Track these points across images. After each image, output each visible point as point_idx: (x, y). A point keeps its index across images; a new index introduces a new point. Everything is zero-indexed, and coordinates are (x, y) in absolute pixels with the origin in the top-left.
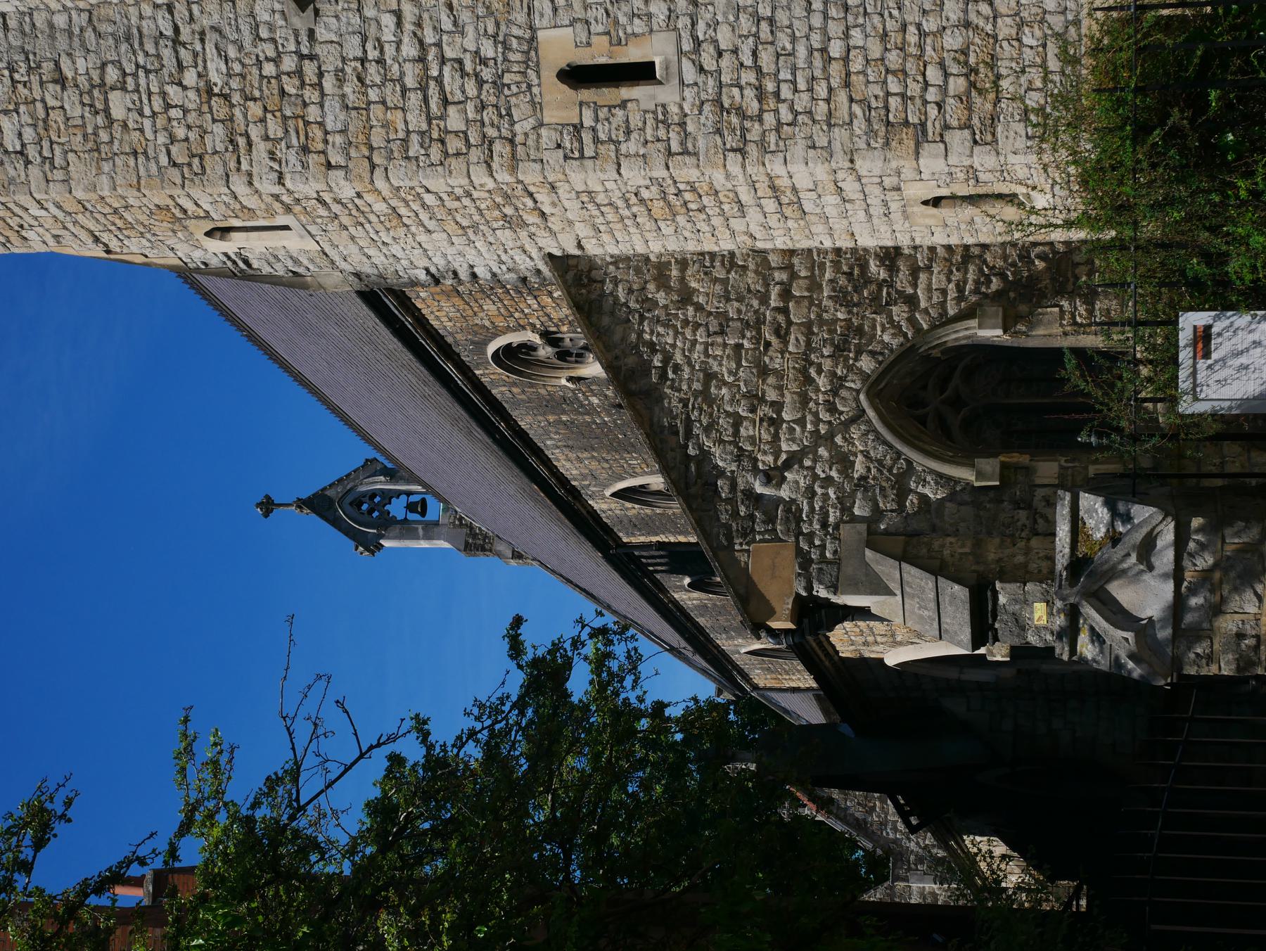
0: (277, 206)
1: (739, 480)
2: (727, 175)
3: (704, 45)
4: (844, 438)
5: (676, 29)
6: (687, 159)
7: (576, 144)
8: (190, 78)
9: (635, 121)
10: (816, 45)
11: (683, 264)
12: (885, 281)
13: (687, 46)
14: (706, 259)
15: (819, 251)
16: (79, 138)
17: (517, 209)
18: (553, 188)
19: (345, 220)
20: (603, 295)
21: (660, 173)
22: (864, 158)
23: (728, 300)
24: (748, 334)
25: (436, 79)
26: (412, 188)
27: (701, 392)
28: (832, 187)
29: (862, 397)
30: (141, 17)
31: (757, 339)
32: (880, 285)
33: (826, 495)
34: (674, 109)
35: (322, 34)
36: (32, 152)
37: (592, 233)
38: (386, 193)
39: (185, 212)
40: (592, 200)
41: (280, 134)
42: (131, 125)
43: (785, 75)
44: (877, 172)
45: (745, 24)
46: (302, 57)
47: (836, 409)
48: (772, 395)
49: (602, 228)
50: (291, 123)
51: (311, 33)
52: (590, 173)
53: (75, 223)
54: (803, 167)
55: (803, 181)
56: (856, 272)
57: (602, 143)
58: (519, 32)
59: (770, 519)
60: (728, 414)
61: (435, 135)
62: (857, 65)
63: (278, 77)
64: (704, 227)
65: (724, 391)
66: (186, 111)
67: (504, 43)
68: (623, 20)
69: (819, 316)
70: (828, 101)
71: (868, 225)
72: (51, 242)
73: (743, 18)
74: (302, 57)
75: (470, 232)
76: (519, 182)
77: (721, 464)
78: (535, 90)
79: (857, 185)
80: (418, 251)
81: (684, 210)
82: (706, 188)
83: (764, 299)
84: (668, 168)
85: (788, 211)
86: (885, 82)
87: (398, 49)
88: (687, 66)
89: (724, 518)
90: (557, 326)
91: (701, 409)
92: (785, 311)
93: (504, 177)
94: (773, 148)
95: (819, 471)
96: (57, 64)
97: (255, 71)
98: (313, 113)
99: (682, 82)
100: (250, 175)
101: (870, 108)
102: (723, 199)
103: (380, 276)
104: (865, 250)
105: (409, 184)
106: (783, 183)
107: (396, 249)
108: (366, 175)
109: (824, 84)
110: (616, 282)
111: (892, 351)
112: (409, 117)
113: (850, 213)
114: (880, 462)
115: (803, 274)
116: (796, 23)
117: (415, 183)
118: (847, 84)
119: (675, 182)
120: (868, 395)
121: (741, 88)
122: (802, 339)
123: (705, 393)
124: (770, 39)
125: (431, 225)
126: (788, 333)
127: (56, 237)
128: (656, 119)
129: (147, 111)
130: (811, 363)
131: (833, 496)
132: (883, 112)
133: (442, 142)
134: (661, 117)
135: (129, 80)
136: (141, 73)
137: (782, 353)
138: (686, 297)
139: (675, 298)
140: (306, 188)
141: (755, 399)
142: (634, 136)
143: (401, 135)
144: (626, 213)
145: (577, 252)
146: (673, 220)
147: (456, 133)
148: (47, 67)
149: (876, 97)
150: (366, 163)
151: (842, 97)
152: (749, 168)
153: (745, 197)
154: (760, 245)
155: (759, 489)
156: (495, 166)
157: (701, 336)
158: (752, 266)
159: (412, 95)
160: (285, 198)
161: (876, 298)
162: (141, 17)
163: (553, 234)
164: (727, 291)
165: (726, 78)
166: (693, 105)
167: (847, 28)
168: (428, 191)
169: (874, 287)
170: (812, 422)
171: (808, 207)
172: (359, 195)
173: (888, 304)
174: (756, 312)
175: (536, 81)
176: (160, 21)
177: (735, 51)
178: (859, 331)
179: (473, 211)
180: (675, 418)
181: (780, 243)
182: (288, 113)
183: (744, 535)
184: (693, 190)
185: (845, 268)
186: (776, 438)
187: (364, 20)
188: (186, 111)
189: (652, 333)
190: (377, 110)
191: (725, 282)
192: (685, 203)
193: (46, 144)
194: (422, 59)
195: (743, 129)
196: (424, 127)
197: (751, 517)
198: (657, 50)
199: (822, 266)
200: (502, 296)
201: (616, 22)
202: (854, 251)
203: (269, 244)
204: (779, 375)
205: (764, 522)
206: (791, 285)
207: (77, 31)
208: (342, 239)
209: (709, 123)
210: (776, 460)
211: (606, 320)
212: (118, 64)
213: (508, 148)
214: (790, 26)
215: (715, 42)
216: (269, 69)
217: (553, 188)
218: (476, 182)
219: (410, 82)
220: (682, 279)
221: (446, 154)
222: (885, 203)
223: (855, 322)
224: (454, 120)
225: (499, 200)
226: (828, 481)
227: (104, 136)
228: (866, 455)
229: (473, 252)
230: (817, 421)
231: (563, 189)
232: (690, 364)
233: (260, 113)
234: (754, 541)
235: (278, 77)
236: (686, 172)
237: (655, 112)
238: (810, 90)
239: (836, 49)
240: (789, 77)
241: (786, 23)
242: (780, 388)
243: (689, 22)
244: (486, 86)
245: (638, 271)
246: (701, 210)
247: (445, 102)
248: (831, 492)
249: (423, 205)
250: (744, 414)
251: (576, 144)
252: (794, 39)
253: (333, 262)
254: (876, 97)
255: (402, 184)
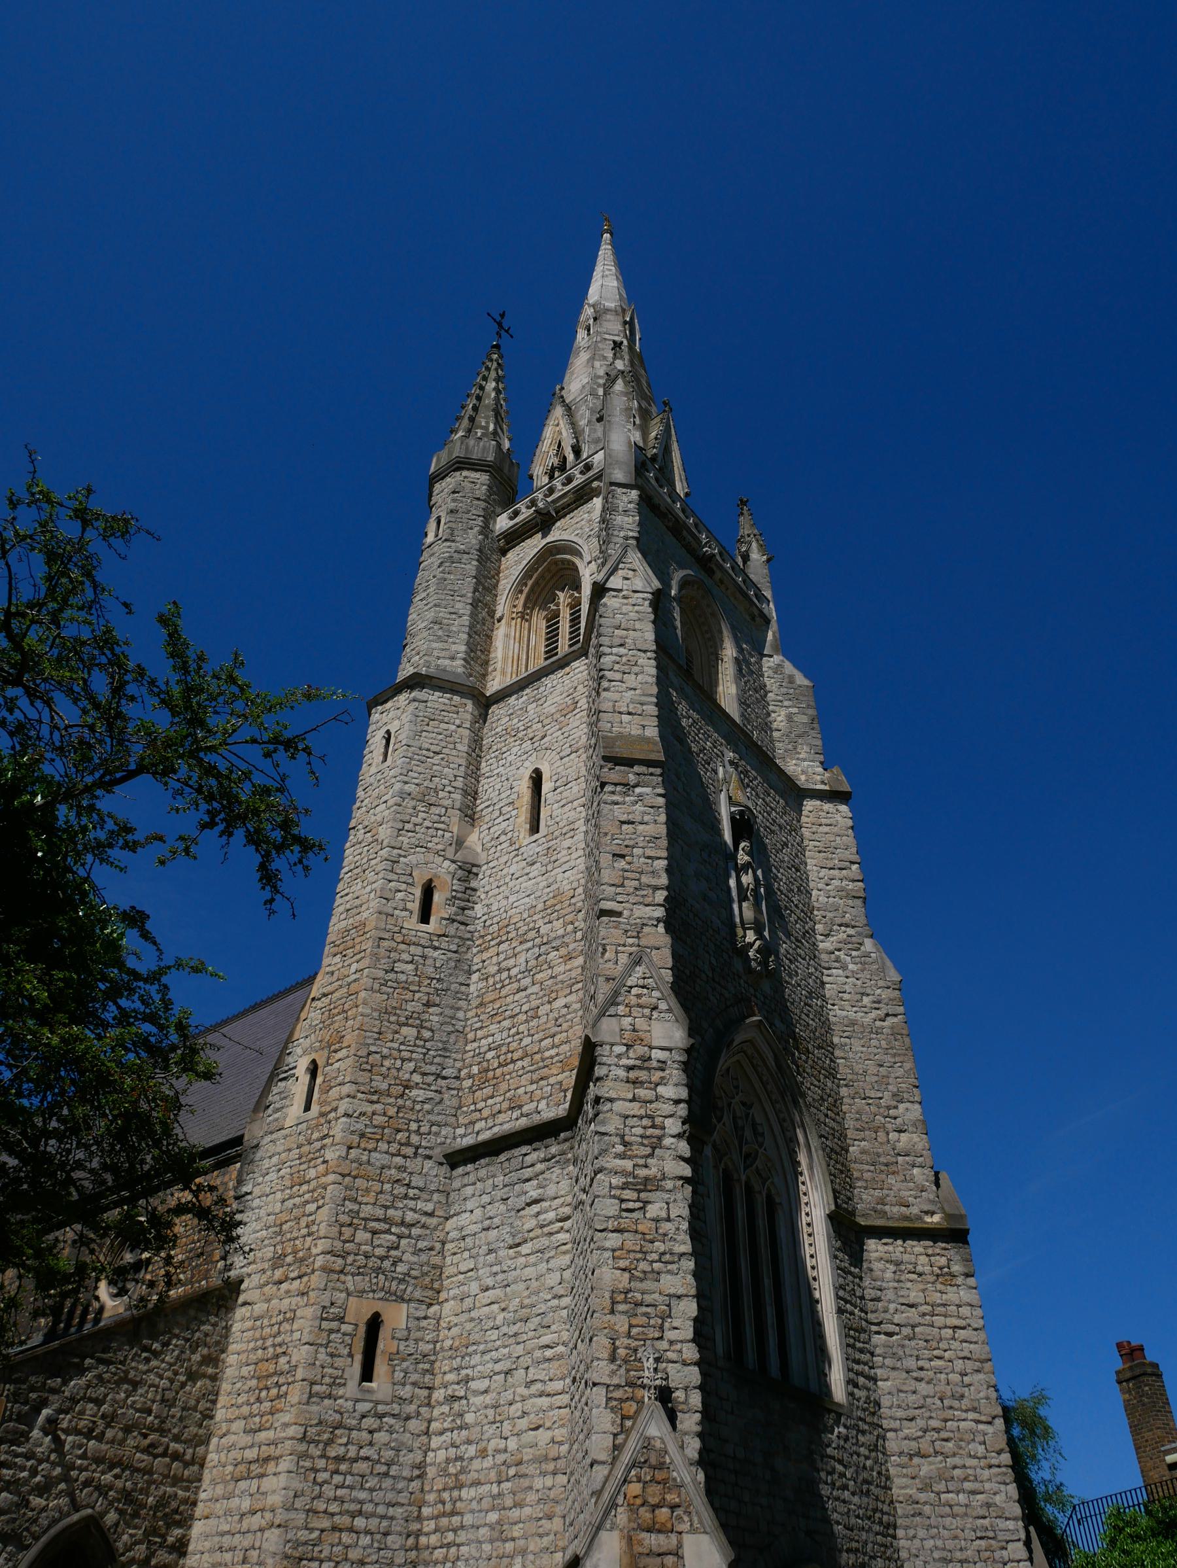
0: (328, 1109)
1: (56, 1397)
2: (287, 1423)
3: (378, 1421)
4: (62, 1491)
5: (393, 1402)
6: (306, 1396)
7: (331, 1316)
8: (417, 1078)
9: (339, 1362)
10: (365, 1507)
11: (214, 1378)
12: (165, 1540)
13: (381, 1408)
14: (212, 1396)
15: (198, 1488)
16: (395, 1004)
17: (289, 1265)
18: (303, 1294)
19: (306, 1149)
20: (209, 1314)
21: (300, 1374)
22: (279, 1536)
23: (183, 1409)
24: (156, 1422)
25: (389, 1229)
26: (323, 1198)
27: (126, 1376)
28: (259, 1506)
29: (89, 1511)
30: (455, 1060)
31: (151, 1429)
32: (163, 1537)
33: (23, 1469)
34: (341, 1392)
35: (428, 1164)
36: (392, 976)
37: (255, 1315)
38: (323, 1180)
39: (335, 1051)
40: (286, 1320)
41: (375, 1122)
42: (397, 1036)
43: (349, 1480)
44: (265, 1546)
45: (388, 1454)
46: (417, 1148)
47: (84, 1487)
48: (109, 1434)
49: (258, 1323)
50: (380, 1131)
51: (429, 1157)
52: (310, 1323)
53: (341, 986)
54: (282, 1485)
55: (268, 1483)
56: (177, 1517)
57: (329, 1336)
58: (408, 1292)
59: (20, 1418)
60: (106, 1395)
61: (355, 1221)
62: (346, 1538)
63: (408, 1130)
64: (240, 1400)
65: (123, 1395)
66: (398, 1070)
67: (404, 1280)
68: (405, 1365)
69: (154, 1482)
70: (325, 1512)
71: (214, 1532)
72: (328, 969)
73: (391, 1453)
74: (417, 1148)
75: (277, 1229)
76: (313, 1271)
77: (72, 1383)
78: (371, 1295)
79: (256, 1527)
80: (268, 1190)
81: (261, 1386)
82: (278, 1406)
83: (177, 1439)
84: (303, 1380)
85: (242, 1468)
86: (330, 1560)
87: (411, 1209)
88: (367, 1406)
89: (33, 1379)
90: (153, 1272)
91: (115, 1374)
92: (164, 1455)
93: (320, 1261)
94: (301, 1463)
95: (44, 1465)
96: (438, 1005)
97: (414, 1117)
98: (383, 1146)
99: (357, 1401)
100: (354, 1097)
101: (314, 1545)
102: (265, 1418)
103: (252, 1161)
104: (190, 1527)
105: (328, 1196)
106: (271, 1467)
107: (272, 1176)
108: (339, 1170)
109: (337, 1510)
110: (215, 1325)
111: (115, 1541)
112: (370, 1207)
113: (230, 1519)
114: (35, 1521)
115: (186, 1473)
116: (381, 1493)
117: (327, 1200)
118: (334, 1529)
119: (289, 1384)
120: (90, 1517)
121: (346, 1445)
122: (142, 1465)
123: (125, 1380)
124: (375, 1472)
125: (289, 1204)
126: (150, 1454)
127: (332, 973)
128: (337, 1377)
129: (402, 1047)
130: (123, 1471)
131: (22, 1475)
132: (309, 1556)
133: (350, 1225)
134: (338, 1381)
135: (422, 1043)
136: (424, 1051)
137: (136, 1447)
138: (192, 1377)
139: (194, 1368)
140: (338, 1129)
141: (110, 1419)
142: (329, 1359)
143: (360, 1199)
144: (269, 1342)
145: (241, 1300)
146: (253, 1377)
147: (354, 1235)
148: (437, 1000)
149: (321, 1551)
150: (347, 1172)
151: (326, 1523)
152: (290, 1442)
153: (263, 1436)
154: (214, 1441)
155: (45, 1412)
156: (328, 1256)
157: (164, 1383)
158: (201, 1432)
159: (382, 1212)
160: (333, 1114)
161: (154, 1531)
162: (455, 1060)
163: (261, 1287)
164: (189, 1409)
165: (354, 1434)
166: (341, 1407)
167: (372, 1534)
168: (318, 1208)
169: (163, 1531)
170: (81, 1465)
171: (243, 1485)
172: (325, 1162)
173: (149, 1541)
174: (170, 1430)
175: (376, 1296)
176: (451, 1070)
177: (371, 1444)
178: (136, 1515)
179: (295, 1234)
180: (115, 1353)
181: (212, 1457)
182: (386, 1131)
183: (15, 1394)
184: (279, 1397)
185: (182, 1508)
186: (78, 1432)
187: (432, 1192)
188: (398, 1070)
189: (176, 1346)
190: (377, 1187)
191: (195, 1409)
192: (268, 1389)
193: (395, 985)
194: (403, 1223)
195: (319, 1442)
196: (362, 1215)
197: (26, 1403)
198: (380, 1385)
199: (187, 1489)
200: (191, 1238)
201: (404, 1360)
202: (192, 1517)
203: (297, 1097)
204: (122, 1442)
205: (19, 1412)
206: (181, 1461)
207: (453, 1022)
208: (291, 1142)
209: (327, 1417)
210: (63, 1430)
211: (192, 1313)
212: (431, 1039)
213: (338, 1268)
214: (380, 1488)
215: (379, 1430)
216: (414, 1126)
217: (303, 1294)
218: (319, 1242)
219: (391, 1212)
220: (204, 1376)
221: (342, 1226)
222: (232, 1549)
223: (143, 1512)
224: (362, 1236)
225: (301, 1254)
226: (34, 1472)
227: (393, 1019)
228: (44, 1509)
229: (258, 1228)
230: (82, 1469)
231: (301, 1301)
232: (149, 1371)
233: (390, 1114)
234: (8, 1401)
235: (408, 1130)
236: (296, 1394)
237: (341, 1377)
238: (335, 1499)
239: (360, 1522)
240: (347, 1483)
241: (383, 1486)
242: (112, 1442)
243: (396, 1412)
244: (379, 1262)
245: (218, 1343)
246: (259, 1400)
247: (374, 1233)
248: (25, 1474)
249: (307, 1202)
250: (102, 1409)
251: (332, 1316)
252: (371, 1490)
253: (271, 1133)
254: (321, 1551)
255: (328, 1191)
